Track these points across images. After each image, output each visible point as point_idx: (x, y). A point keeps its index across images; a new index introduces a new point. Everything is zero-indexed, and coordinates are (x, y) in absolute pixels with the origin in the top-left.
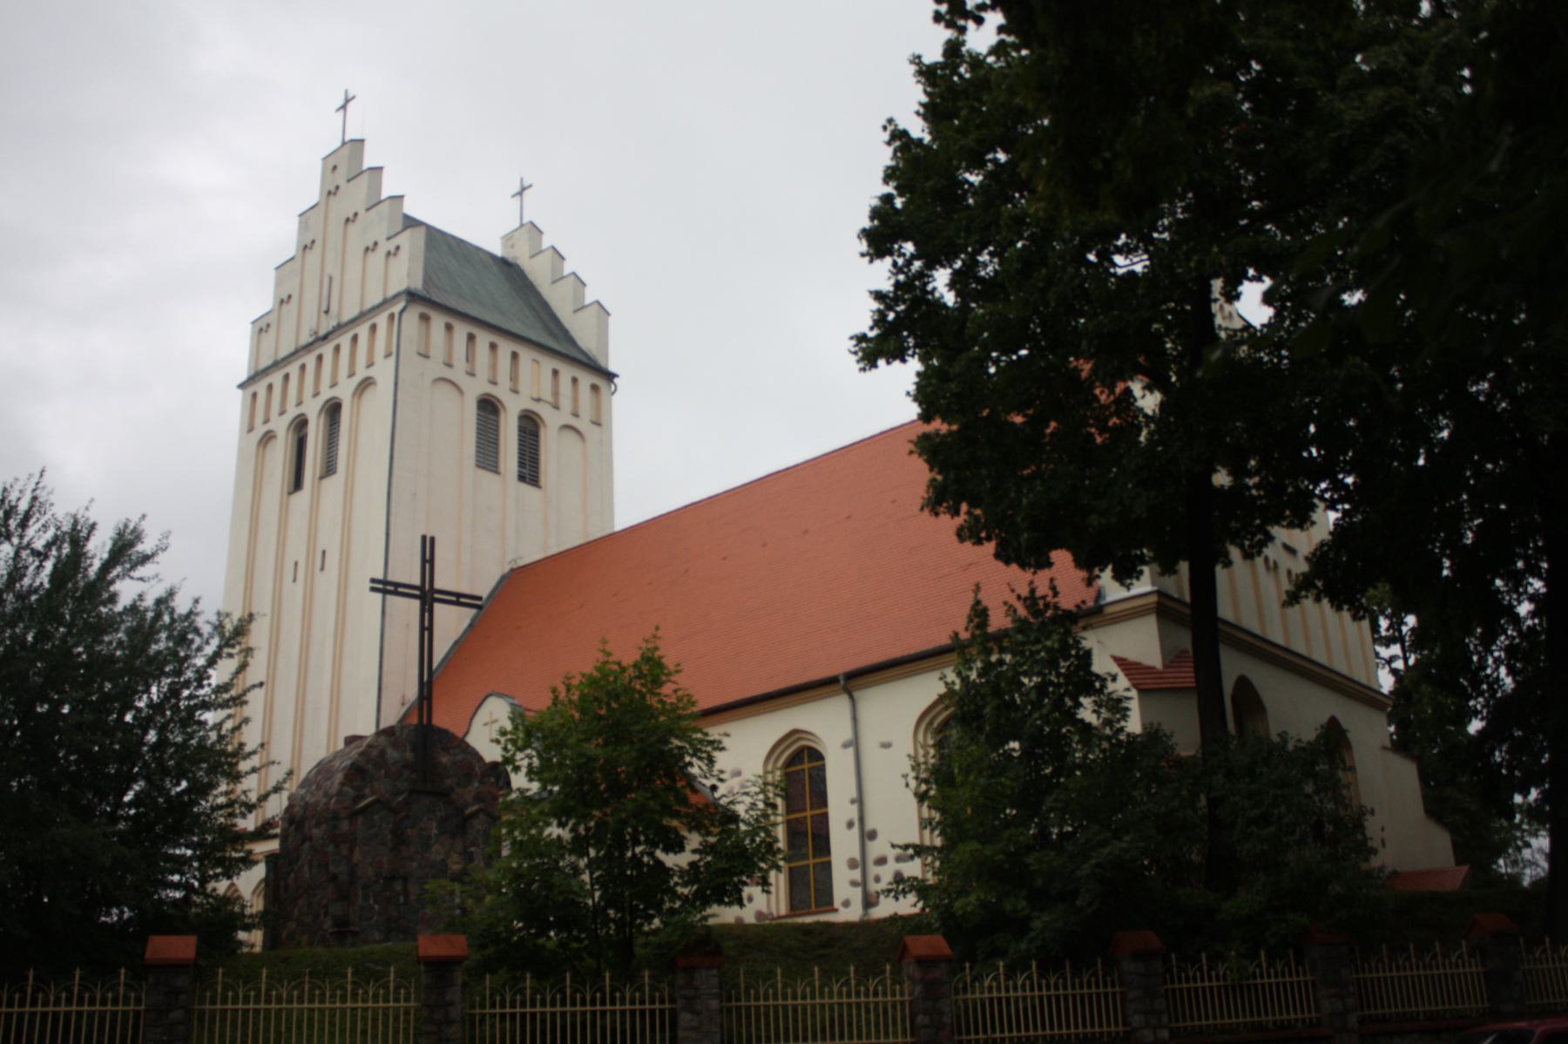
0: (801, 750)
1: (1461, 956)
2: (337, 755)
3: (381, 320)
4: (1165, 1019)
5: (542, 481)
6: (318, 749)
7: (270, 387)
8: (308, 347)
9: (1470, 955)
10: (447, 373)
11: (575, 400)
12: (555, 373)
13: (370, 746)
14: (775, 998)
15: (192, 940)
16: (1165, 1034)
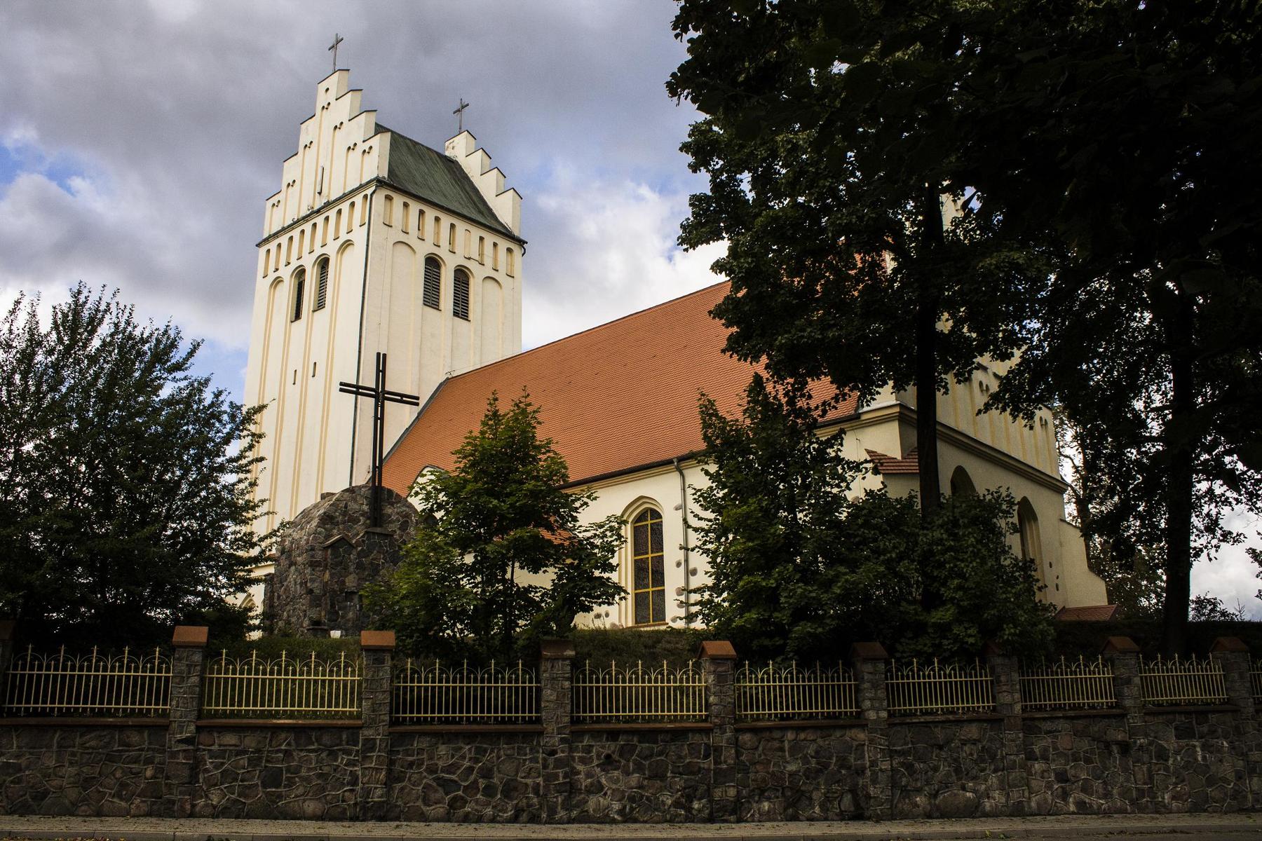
0: (646, 510)
1: (1097, 666)
2: (316, 506)
3: (358, 199)
4: (885, 703)
5: (471, 316)
6: (309, 499)
7: (279, 245)
8: (305, 219)
9: (1104, 666)
10: (403, 238)
11: (495, 259)
12: (481, 239)
13: (337, 500)
14: (610, 682)
15: (206, 629)
16: (884, 714)
